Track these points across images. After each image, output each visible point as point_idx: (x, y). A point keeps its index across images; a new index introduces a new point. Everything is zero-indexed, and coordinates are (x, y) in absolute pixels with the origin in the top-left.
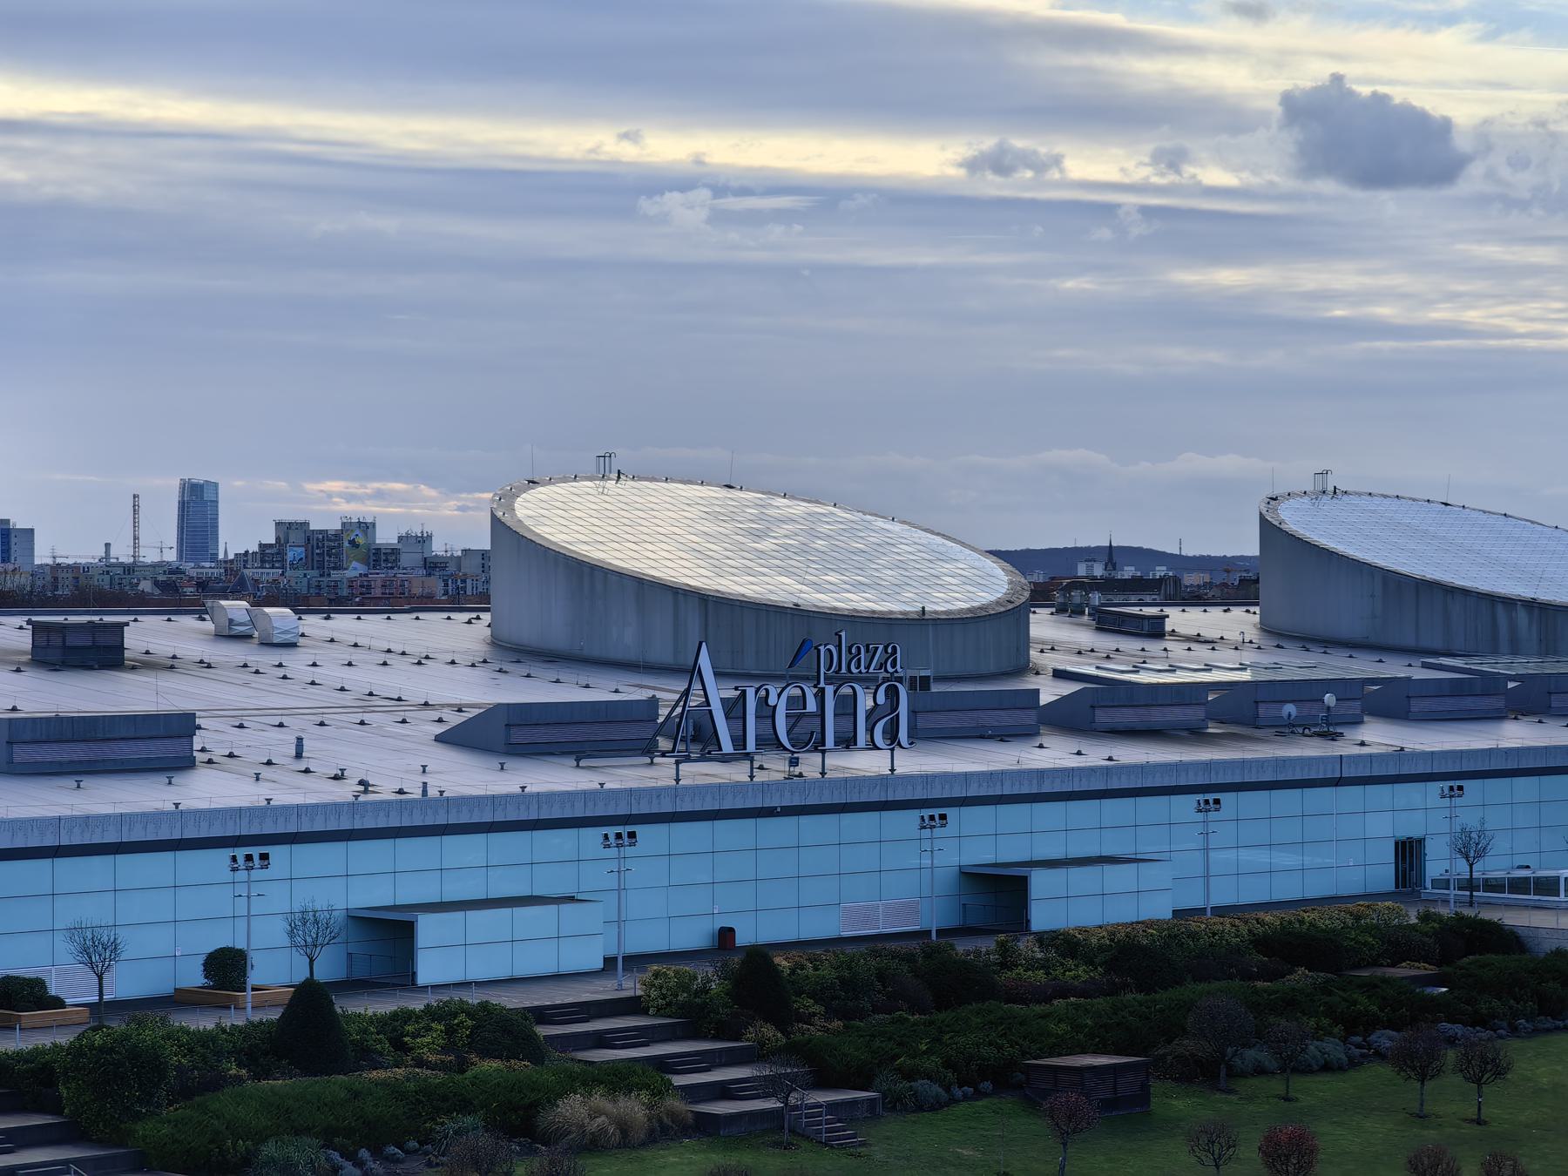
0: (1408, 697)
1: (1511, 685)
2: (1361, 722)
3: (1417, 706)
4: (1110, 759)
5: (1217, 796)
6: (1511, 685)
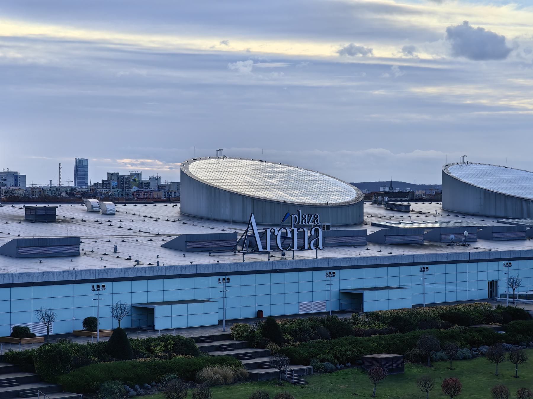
0: (493, 233)
1: (527, 229)
2: (477, 241)
3: (496, 235)
4: (391, 253)
5: (427, 266)
6: (527, 229)
